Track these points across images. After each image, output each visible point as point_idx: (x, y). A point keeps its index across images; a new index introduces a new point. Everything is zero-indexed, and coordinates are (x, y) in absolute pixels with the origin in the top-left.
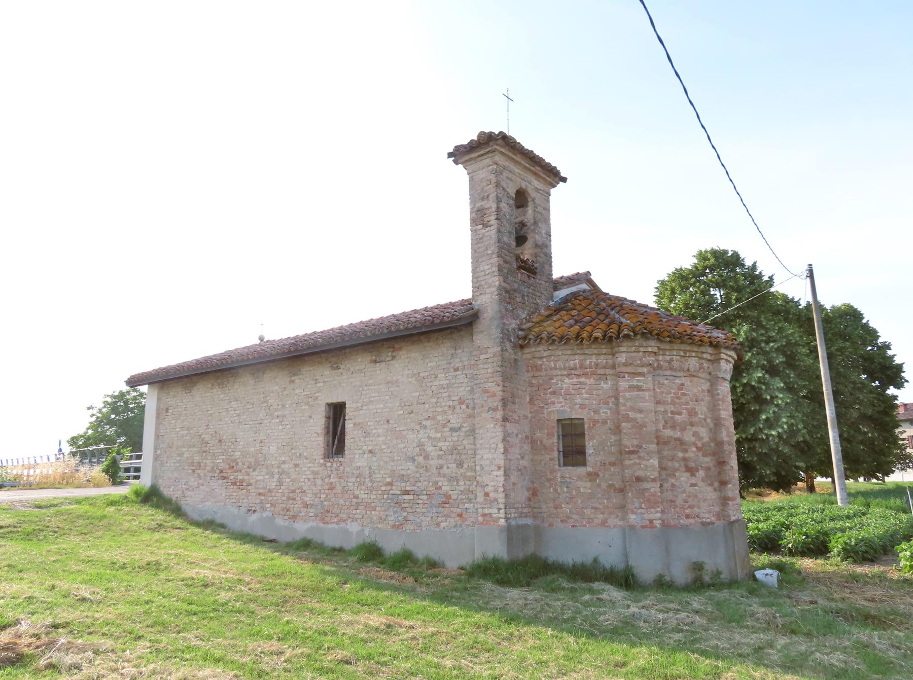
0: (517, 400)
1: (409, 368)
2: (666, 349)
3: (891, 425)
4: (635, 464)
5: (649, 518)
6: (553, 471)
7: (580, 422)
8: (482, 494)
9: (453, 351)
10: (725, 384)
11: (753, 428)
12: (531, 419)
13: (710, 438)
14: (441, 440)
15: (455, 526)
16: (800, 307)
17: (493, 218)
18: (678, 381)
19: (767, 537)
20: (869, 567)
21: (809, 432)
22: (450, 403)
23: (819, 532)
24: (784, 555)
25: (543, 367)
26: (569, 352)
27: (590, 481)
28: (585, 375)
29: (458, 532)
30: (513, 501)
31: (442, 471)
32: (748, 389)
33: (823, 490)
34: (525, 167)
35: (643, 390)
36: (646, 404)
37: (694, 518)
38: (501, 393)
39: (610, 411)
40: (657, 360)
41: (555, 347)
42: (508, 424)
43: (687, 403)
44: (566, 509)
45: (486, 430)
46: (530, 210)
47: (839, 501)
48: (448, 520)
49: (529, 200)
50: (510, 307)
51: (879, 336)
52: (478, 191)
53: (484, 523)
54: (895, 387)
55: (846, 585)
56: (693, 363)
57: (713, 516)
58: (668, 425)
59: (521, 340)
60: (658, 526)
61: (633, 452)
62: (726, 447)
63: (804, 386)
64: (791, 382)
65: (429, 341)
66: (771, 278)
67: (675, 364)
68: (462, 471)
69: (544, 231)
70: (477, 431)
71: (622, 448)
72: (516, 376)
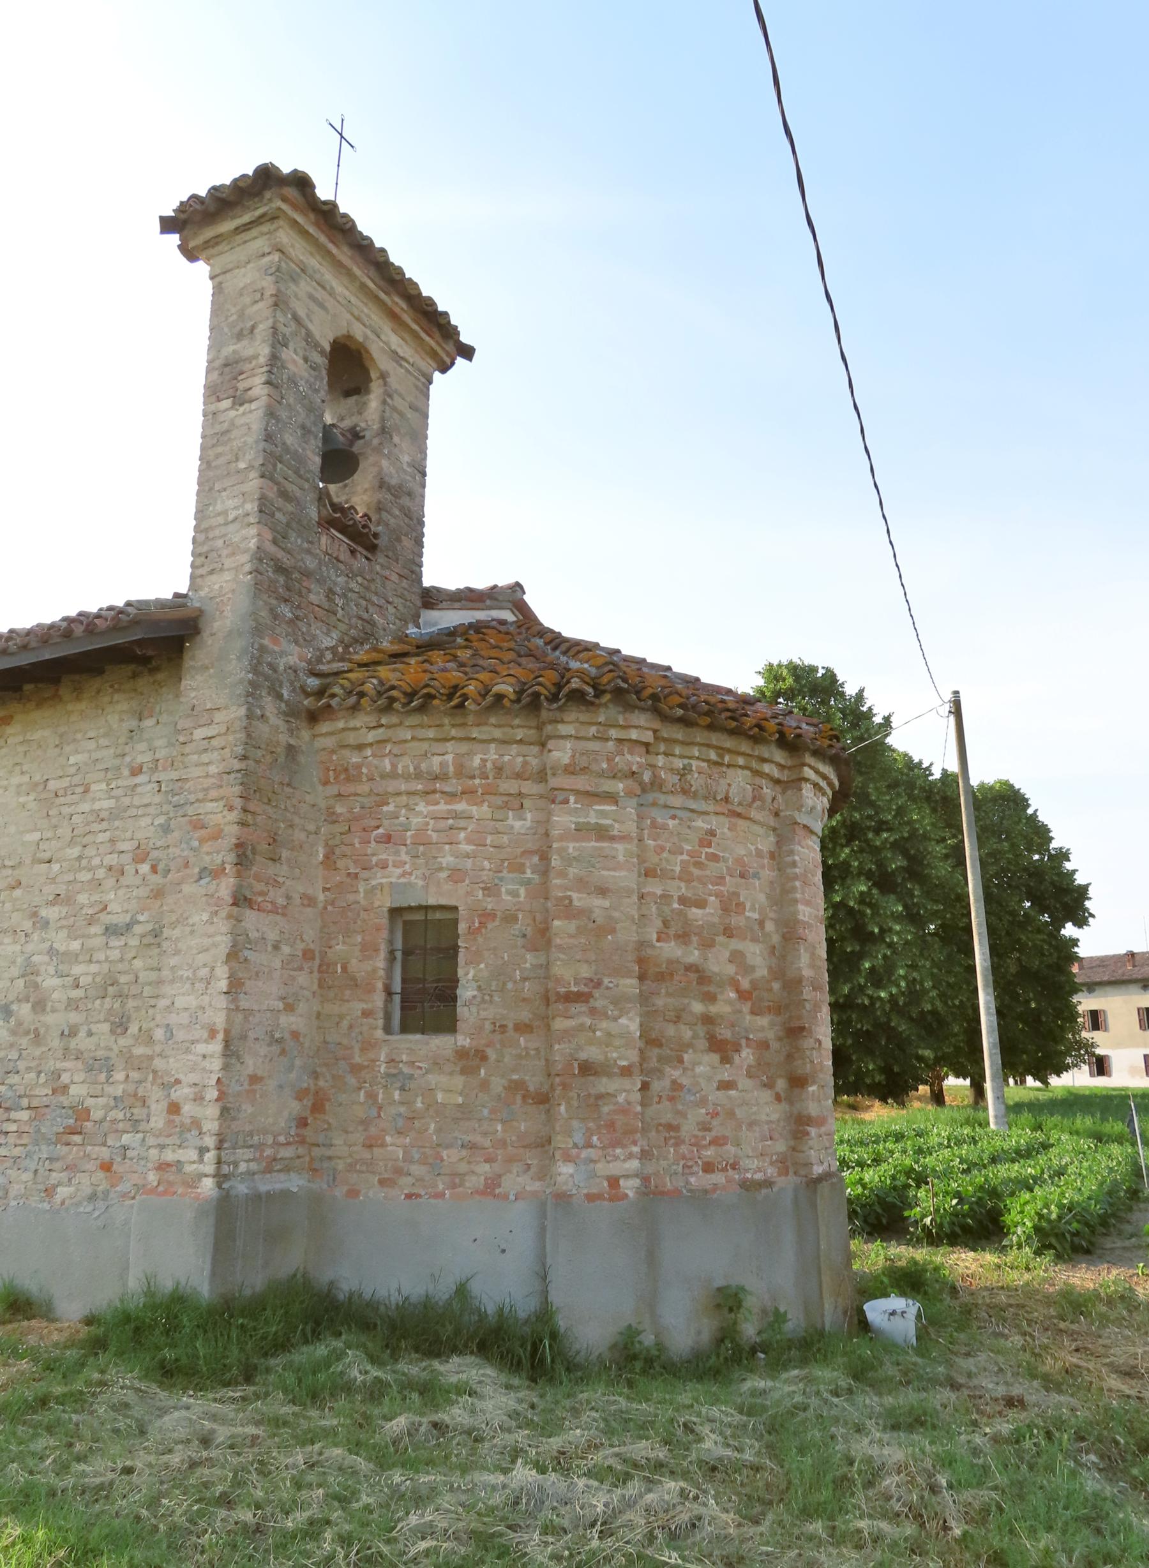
0: (285, 854)
1: (25, 768)
2: (675, 741)
3: (1067, 989)
4: (581, 1028)
5: (608, 1173)
6: (368, 1045)
7: (448, 916)
8: (164, 1105)
9: (134, 723)
10: (811, 843)
11: (849, 985)
12: (325, 908)
13: (770, 968)
14: (81, 958)
15: (93, 1197)
16: (930, 778)
17: (259, 380)
18: (699, 823)
19: (881, 1201)
20: (1088, 1269)
21: (943, 996)
22: (112, 860)
23: (981, 1188)
24: (916, 1242)
25: (364, 770)
26: (431, 734)
27: (464, 1071)
28: (468, 793)
29: (97, 1213)
30: (248, 1128)
31: (73, 1044)
32: (842, 914)
33: (955, 1099)
34: (363, 286)
35: (612, 839)
36: (617, 874)
37: (725, 1170)
38: (235, 829)
39: (526, 890)
40: (653, 766)
41: (394, 719)
42: (251, 918)
43: (720, 880)
44: (394, 1147)
45: (188, 929)
46: (373, 401)
47: (992, 1120)
48: (74, 1181)
49: (374, 375)
50: (286, 611)
51: (1052, 838)
52: (231, 319)
53: (161, 1189)
54: (1074, 925)
55: (1062, 1325)
56: (738, 783)
57: (772, 1163)
58: (672, 932)
59: (311, 699)
60: (631, 1194)
61: (571, 998)
62: (807, 993)
63: (937, 911)
64: (914, 904)
65: (78, 699)
66: (887, 720)
67: (696, 781)
68: (123, 1042)
69: (406, 459)
70: (166, 932)
71: (551, 985)
72: (288, 790)
